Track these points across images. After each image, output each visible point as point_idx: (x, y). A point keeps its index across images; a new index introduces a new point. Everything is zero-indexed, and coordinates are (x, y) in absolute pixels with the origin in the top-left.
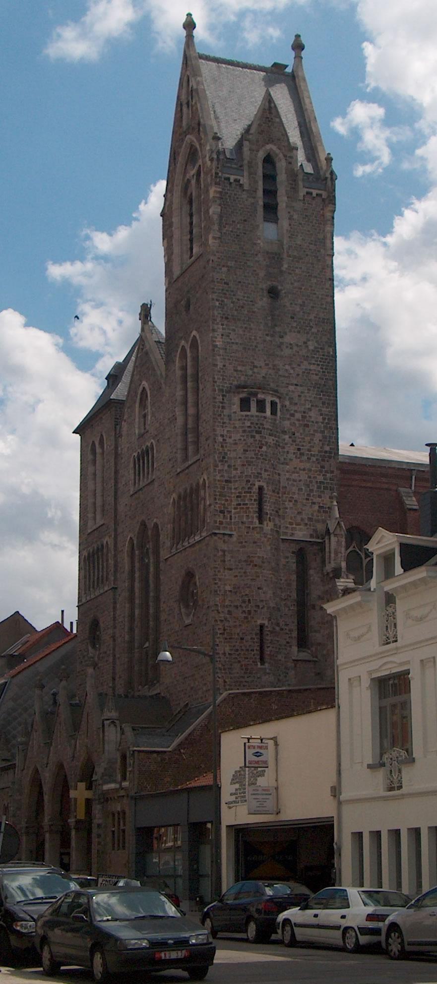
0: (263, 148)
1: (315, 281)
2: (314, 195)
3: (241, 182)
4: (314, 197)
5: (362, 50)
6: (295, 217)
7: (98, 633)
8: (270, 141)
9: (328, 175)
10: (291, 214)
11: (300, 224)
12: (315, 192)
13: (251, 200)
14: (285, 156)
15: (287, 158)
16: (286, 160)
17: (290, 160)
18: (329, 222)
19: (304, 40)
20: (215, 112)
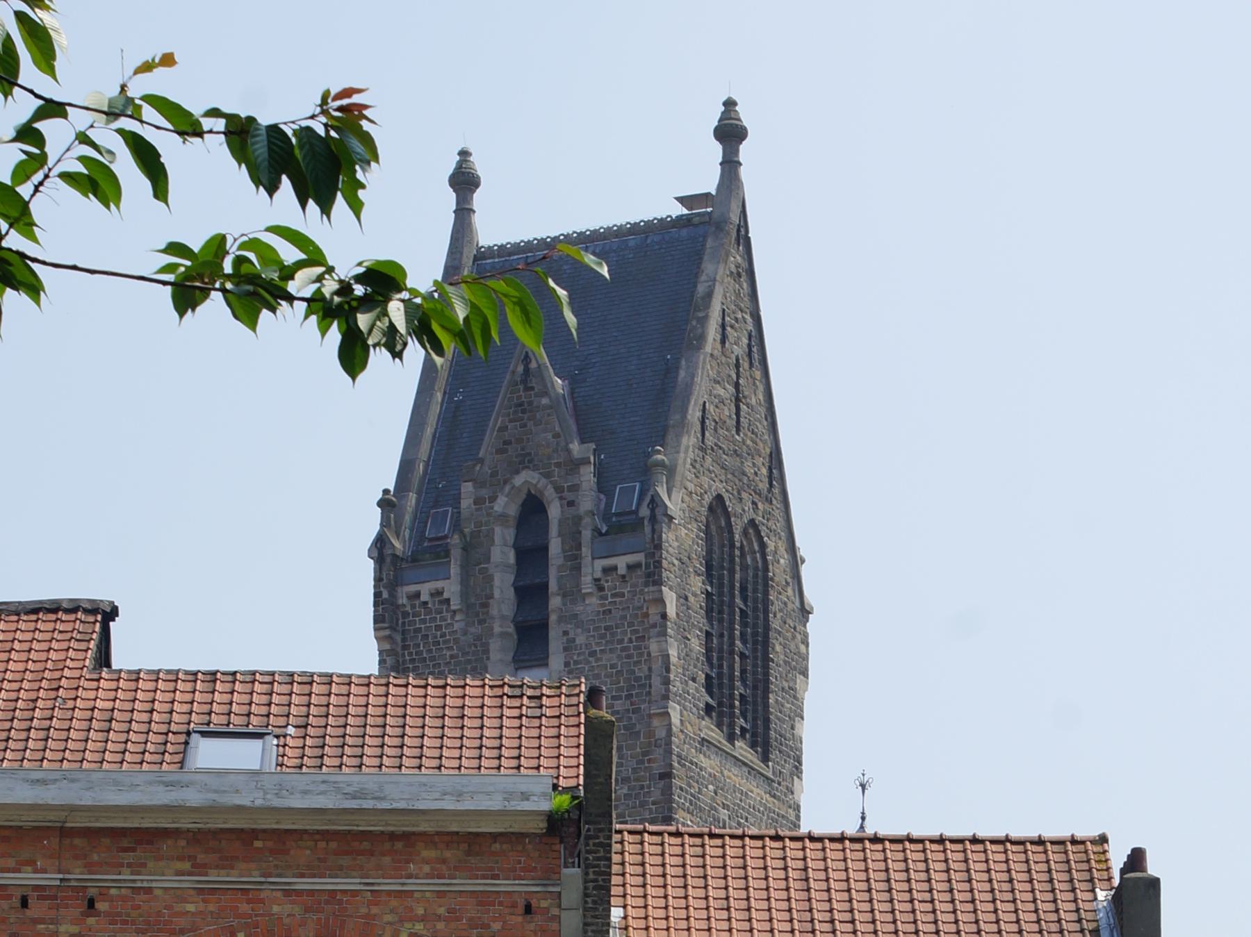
0: (507, 488)
1: (625, 791)
2: (622, 570)
3: (446, 595)
4: (623, 576)
5: (361, 126)
6: (581, 640)
7: (410, 475)
8: (526, 461)
9: (645, 512)
10: (571, 635)
11: (593, 654)
12: (621, 562)
13: (475, 630)
14: (558, 489)
15: (566, 493)
16: (561, 498)
17: (570, 496)
18: (654, 631)
19: (479, 164)
20: (115, 817)
